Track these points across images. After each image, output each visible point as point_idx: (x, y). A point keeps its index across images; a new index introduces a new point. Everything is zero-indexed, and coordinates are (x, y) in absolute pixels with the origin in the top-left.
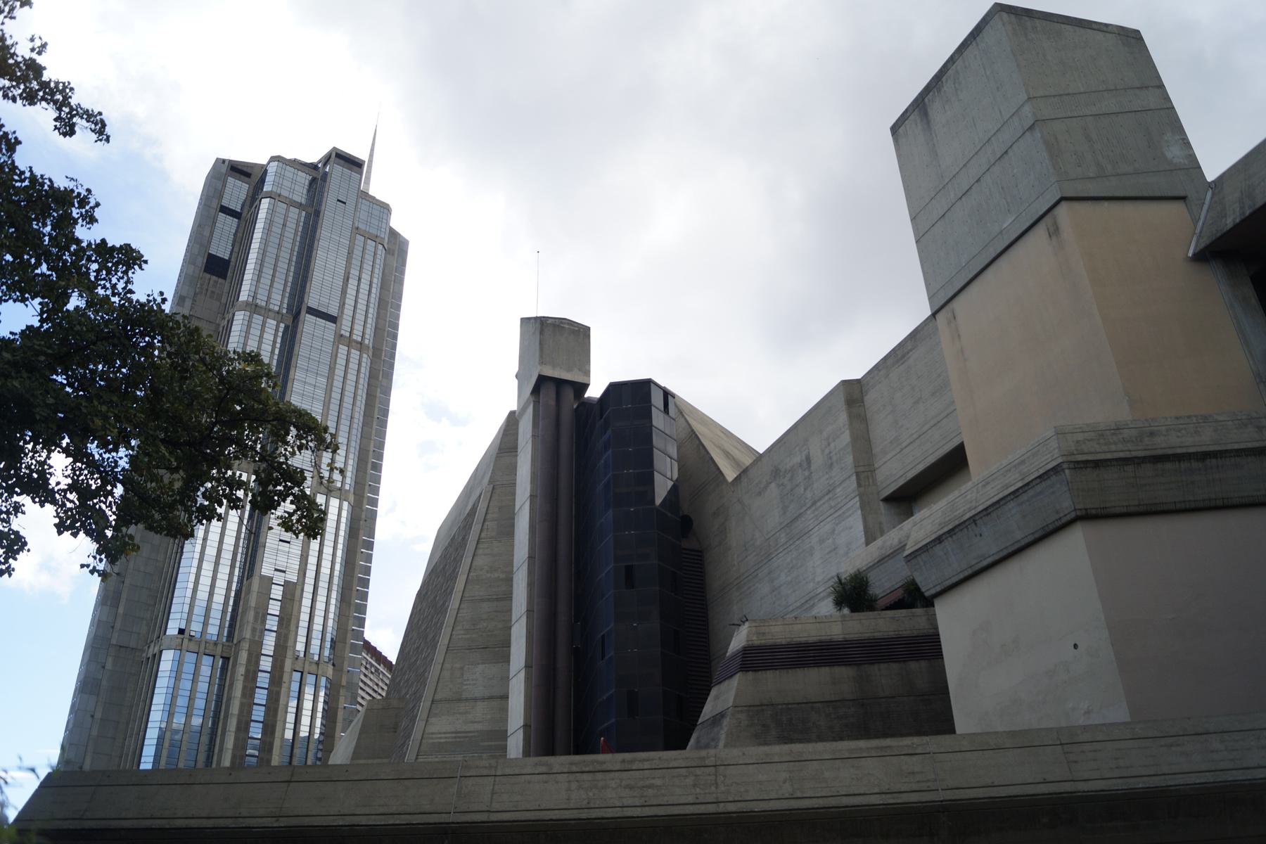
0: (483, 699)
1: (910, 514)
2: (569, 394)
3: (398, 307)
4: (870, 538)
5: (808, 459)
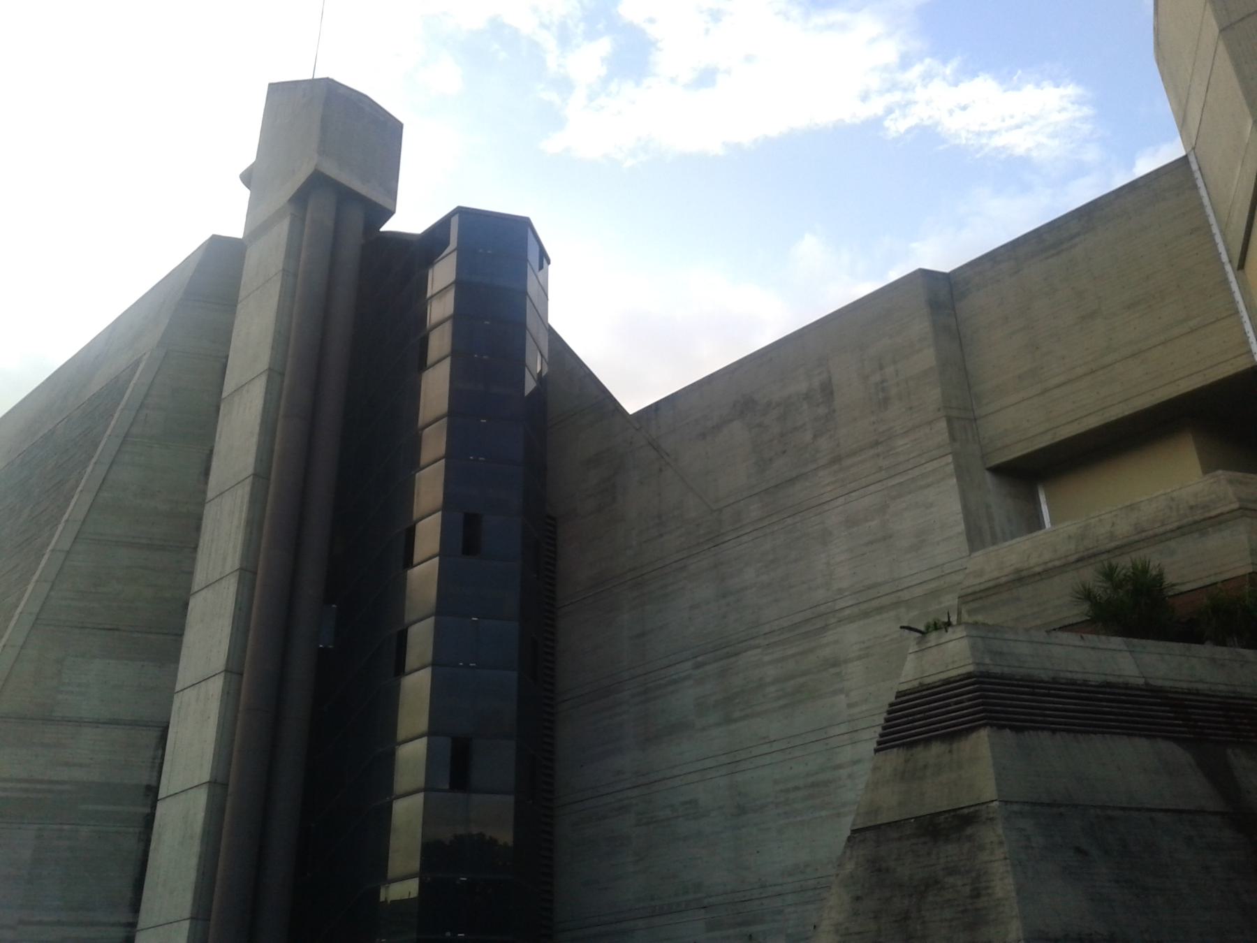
0: (96, 723)
4: (976, 537)
5: (828, 390)
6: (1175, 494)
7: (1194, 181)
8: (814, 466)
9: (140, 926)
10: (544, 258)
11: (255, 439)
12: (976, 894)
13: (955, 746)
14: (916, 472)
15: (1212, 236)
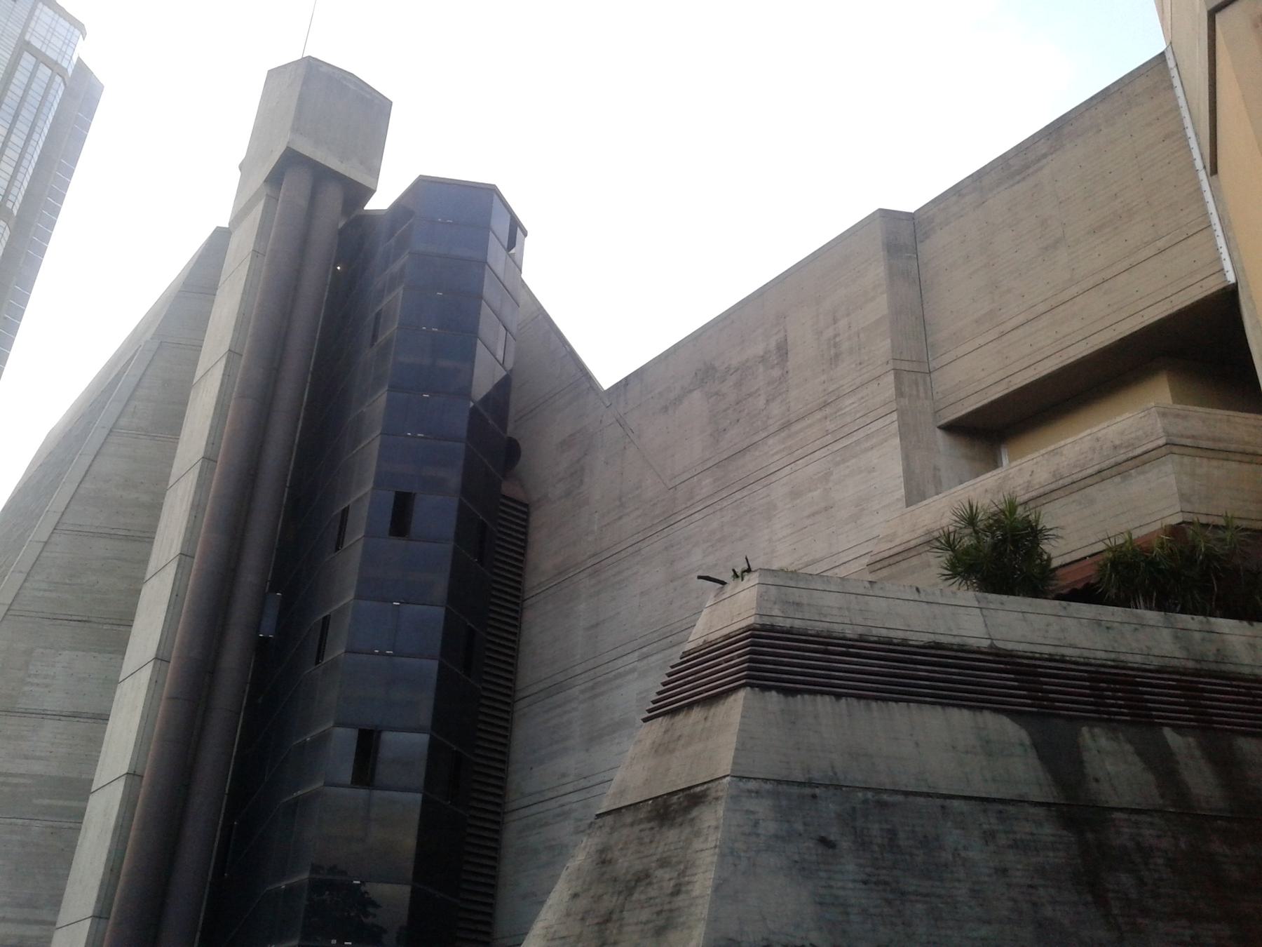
0: (60, 716)
1: (995, 463)
2: (332, 198)
3: (70, 173)
4: (914, 495)
5: (783, 350)
6: (1100, 435)
7: (1170, 80)
8: (764, 435)
10: (515, 230)
11: (208, 422)
12: (676, 892)
13: (713, 710)
14: (861, 434)
15: (1186, 139)
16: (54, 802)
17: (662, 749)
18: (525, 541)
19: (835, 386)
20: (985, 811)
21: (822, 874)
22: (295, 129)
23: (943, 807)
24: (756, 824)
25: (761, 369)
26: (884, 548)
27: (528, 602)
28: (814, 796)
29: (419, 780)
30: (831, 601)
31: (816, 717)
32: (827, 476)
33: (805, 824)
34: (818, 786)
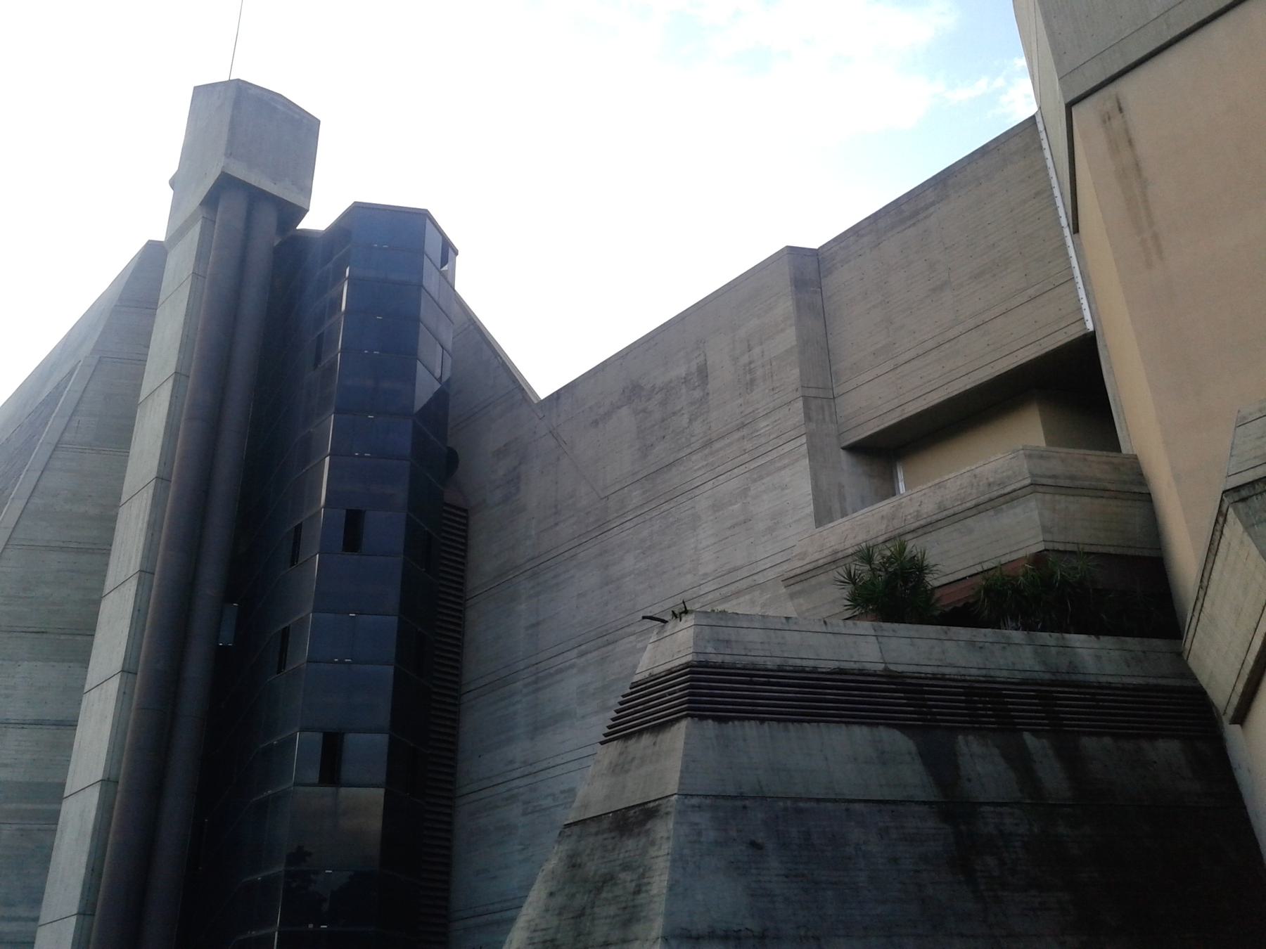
0: (22, 724)
2: (267, 220)
4: (823, 515)
5: (703, 373)
6: (977, 471)
7: (1040, 141)
8: (689, 450)
9: (41, 922)
10: (448, 251)
12: (638, 891)
13: (661, 737)
14: (774, 454)
16: (24, 806)
17: (618, 769)
18: (465, 544)
19: (750, 409)
20: (880, 811)
21: (754, 871)
22: (230, 154)
23: (847, 810)
24: (699, 834)
25: (684, 391)
26: (797, 565)
27: (469, 603)
28: (745, 807)
29: (382, 777)
30: (754, 636)
31: (745, 740)
32: (745, 492)
33: (739, 831)
34: (747, 798)
